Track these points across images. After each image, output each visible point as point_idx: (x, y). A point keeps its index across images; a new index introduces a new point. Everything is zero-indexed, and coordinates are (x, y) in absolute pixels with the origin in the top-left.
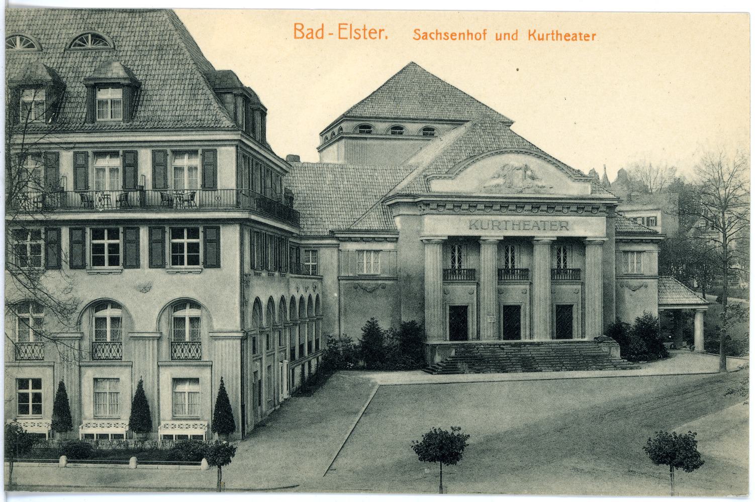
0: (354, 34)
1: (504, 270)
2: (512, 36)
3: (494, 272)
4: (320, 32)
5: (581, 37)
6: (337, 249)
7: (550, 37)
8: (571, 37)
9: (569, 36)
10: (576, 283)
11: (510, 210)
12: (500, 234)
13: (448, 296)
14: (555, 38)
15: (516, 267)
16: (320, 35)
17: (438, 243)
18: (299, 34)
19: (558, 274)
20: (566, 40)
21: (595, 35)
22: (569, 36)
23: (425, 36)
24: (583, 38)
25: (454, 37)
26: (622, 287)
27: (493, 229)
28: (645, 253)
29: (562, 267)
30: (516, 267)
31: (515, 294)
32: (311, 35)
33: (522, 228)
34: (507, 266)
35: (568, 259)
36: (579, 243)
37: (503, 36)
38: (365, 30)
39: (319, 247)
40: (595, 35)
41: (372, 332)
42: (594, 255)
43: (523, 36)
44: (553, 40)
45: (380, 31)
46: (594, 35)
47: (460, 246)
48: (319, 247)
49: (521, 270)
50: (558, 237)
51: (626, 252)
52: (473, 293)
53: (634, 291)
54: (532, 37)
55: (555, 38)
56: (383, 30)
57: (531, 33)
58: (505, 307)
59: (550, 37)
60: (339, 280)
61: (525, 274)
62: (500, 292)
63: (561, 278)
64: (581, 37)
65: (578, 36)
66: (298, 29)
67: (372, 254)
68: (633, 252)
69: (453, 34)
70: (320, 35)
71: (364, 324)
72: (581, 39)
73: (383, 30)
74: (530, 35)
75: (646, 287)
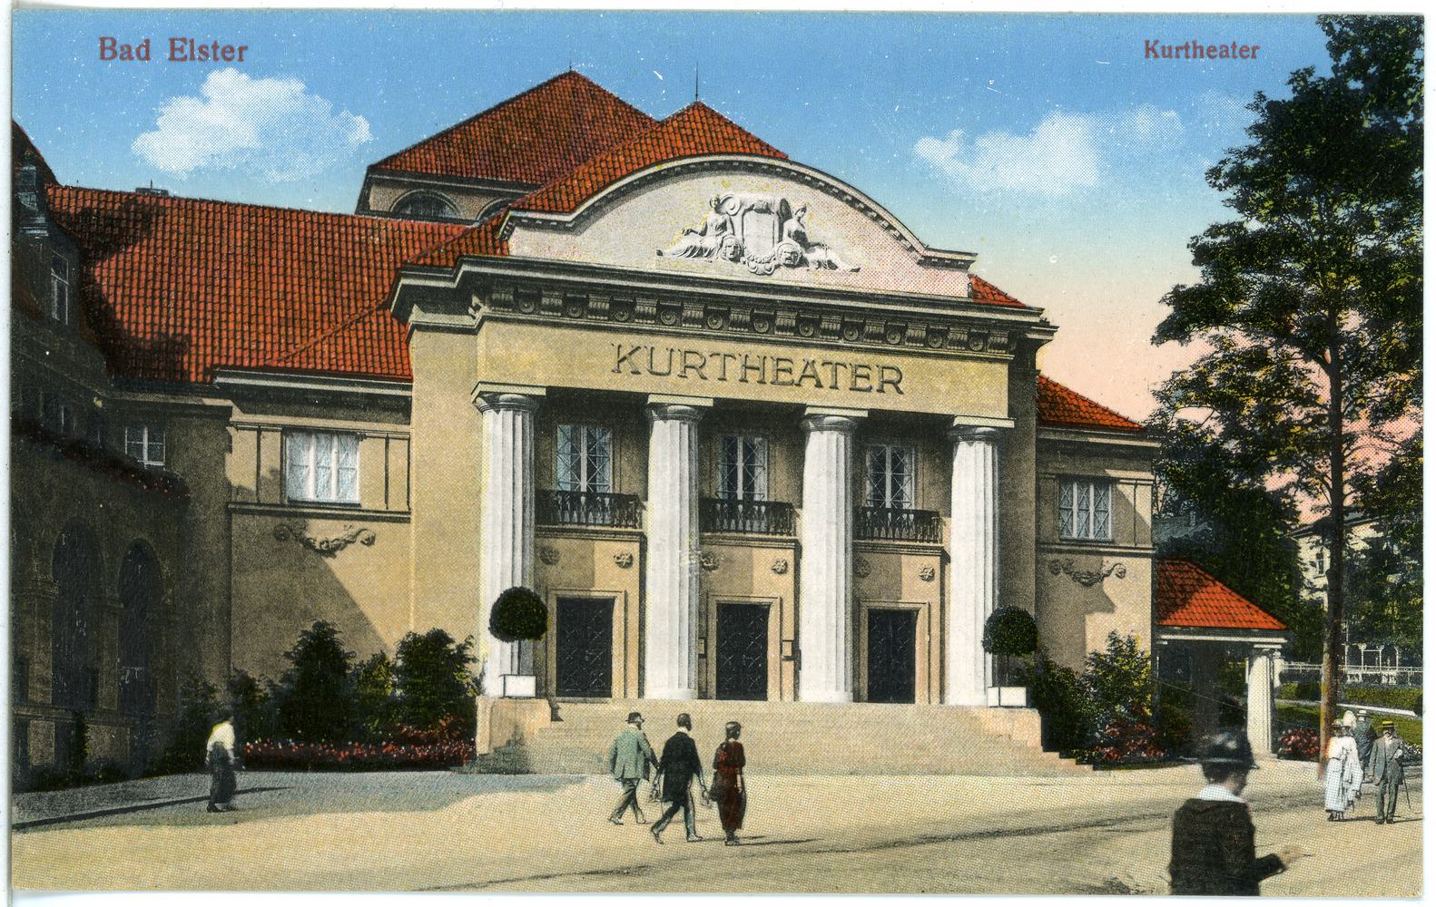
1: (722, 501)
3: (972, 522)
4: (143, 49)
7: (1182, 53)
8: (1219, 51)
9: (1215, 50)
10: (782, 545)
11: (911, 339)
12: (704, 393)
13: (552, 569)
17: (514, 406)
19: (715, 515)
21: (246, 48)
22: (1215, 50)
23: (1168, 53)
25: (229, 55)
27: (881, 391)
30: (906, 506)
32: (127, 54)
33: (769, 377)
36: (935, 437)
40: (246, 48)
42: (972, 469)
43: (161, 52)
44: (1187, 57)
45: (241, 49)
46: (241, 49)
50: (871, 411)
54: (1151, 54)
57: (1151, 45)
59: (1182, 53)
60: (229, 513)
62: (706, 565)
63: (733, 527)
65: (1230, 51)
66: (110, 49)
69: (1212, 49)
70: (143, 54)
71: (292, 642)
74: (1148, 49)
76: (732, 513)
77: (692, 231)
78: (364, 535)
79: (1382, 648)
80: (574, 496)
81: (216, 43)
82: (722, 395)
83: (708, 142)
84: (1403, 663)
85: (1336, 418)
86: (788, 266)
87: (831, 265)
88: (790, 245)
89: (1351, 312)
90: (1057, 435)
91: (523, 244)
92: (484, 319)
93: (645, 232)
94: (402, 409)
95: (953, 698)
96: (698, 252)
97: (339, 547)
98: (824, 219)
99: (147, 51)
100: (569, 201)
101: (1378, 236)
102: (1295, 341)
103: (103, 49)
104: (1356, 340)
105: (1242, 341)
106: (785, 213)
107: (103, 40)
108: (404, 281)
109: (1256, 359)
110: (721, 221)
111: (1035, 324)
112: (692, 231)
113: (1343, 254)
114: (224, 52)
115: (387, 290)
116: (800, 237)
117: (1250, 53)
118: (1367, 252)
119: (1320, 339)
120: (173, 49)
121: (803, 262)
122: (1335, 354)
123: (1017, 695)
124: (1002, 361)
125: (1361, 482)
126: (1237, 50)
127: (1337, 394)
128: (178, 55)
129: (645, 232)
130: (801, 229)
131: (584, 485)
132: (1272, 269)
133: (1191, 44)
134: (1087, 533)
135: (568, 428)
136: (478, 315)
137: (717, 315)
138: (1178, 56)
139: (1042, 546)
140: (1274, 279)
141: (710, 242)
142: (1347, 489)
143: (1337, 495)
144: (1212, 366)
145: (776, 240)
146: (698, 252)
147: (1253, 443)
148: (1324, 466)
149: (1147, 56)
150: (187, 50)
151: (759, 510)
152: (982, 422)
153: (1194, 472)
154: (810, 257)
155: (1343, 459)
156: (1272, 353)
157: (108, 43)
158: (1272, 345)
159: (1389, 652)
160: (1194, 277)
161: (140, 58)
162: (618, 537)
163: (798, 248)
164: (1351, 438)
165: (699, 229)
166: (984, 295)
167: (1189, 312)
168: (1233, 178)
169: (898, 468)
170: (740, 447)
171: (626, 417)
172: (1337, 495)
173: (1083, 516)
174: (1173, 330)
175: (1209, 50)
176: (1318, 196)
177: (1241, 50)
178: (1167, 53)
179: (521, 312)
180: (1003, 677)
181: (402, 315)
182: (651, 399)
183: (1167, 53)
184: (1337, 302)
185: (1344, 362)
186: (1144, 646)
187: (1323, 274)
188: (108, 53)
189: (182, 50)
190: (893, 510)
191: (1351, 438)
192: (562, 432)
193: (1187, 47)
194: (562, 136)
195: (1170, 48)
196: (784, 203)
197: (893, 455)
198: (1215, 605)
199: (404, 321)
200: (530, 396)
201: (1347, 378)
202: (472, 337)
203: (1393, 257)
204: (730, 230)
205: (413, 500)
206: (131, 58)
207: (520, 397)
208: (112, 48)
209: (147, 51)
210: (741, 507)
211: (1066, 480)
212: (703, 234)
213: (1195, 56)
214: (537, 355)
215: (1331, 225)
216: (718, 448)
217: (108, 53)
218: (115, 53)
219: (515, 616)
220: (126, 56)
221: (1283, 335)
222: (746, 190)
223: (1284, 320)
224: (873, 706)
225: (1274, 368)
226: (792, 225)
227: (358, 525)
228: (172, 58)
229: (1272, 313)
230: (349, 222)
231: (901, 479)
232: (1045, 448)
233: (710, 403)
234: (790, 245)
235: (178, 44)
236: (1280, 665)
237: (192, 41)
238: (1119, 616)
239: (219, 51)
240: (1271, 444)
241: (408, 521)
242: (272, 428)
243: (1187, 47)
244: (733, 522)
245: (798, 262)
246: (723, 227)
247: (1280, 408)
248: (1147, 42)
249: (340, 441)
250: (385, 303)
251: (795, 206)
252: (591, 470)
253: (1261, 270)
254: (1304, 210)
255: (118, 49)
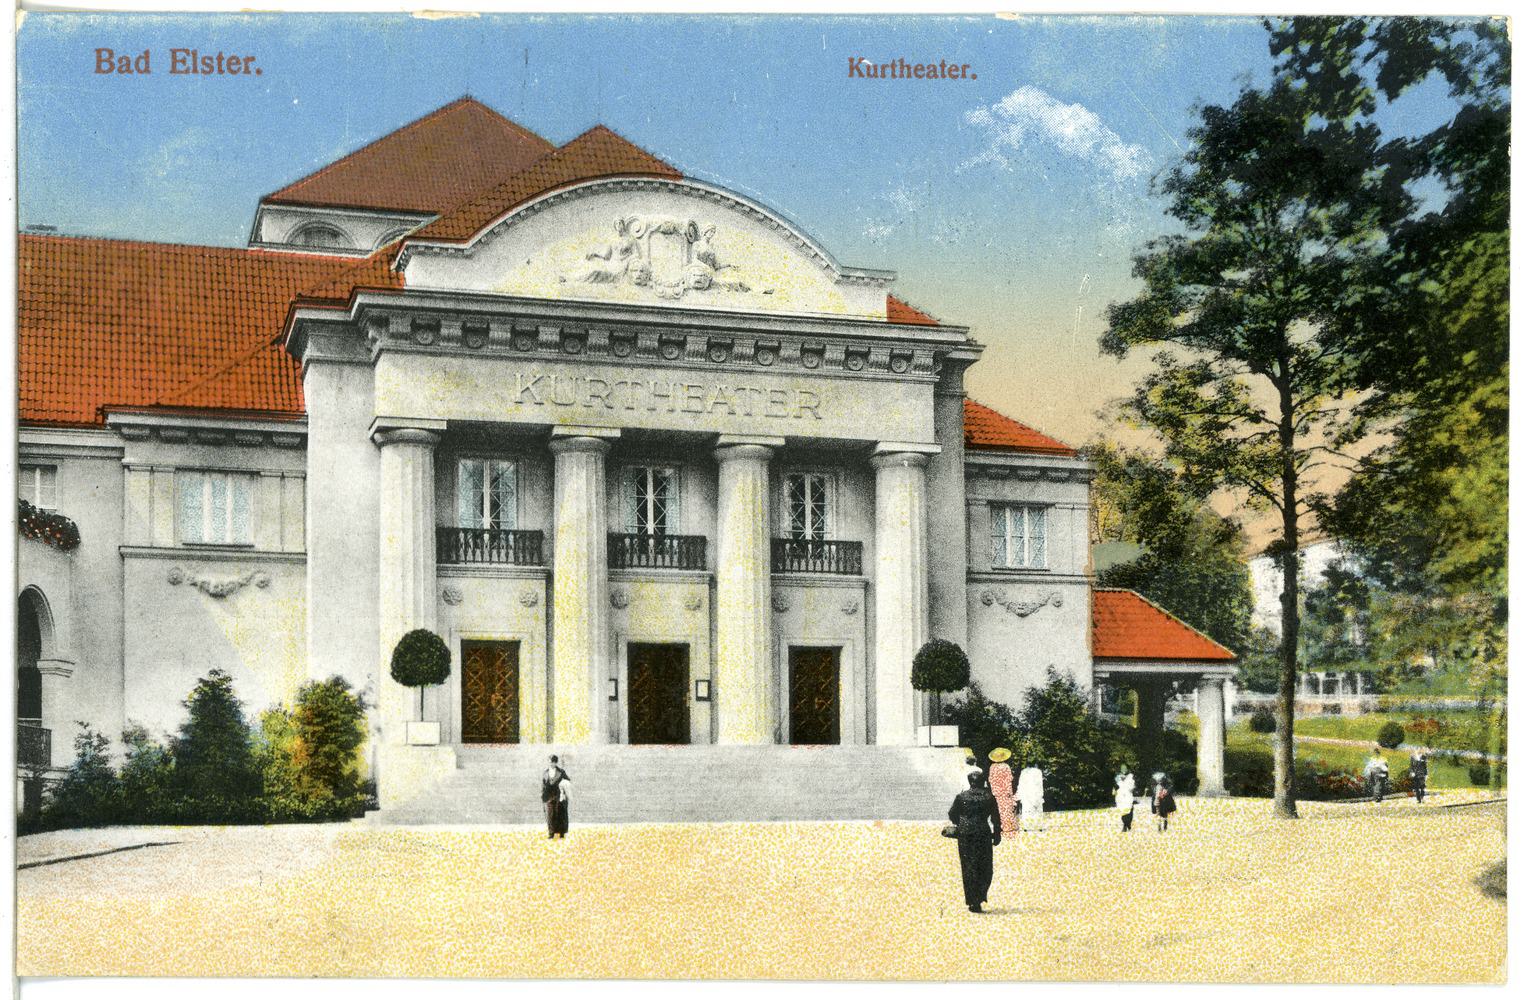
0: (200, 66)
1: (632, 537)
2: (137, 63)
4: (142, 61)
5: (220, 65)
6: (115, 464)
7: (888, 71)
8: (926, 71)
9: (923, 69)
13: (455, 611)
14: (897, 73)
15: (827, 537)
16: (142, 65)
18: (180, 67)
19: (787, 555)
20: (917, 76)
22: (923, 69)
23: (873, 73)
24: (224, 66)
26: (988, 603)
28: (1051, 511)
29: (651, 531)
30: (827, 537)
31: (662, 609)
32: (126, 67)
34: (642, 529)
35: (671, 510)
36: (856, 463)
37: (879, 70)
38: (943, 65)
39: (62, 457)
41: (214, 706)
42: (898, 494)
47: (822, 482)
48: (62, 457)
49: (521, 535)
51: (997, 506)
52: (854, 611)
53: (1022, 616)
54: (855, 72)
55: (897, 73)
56: (253, 59)
58: (792, 649)
59: (888, 71)
61: (694, 553)
64: (220, 65)
66: (106, 61)
67: (1008, 510)
68: (1017, 507)
70: (142, 65)
72: (221, 71)
73: (253, 59)
74: (852, 68)
75: (1058, 605)
76: (644, 549)
77: (596, 256)
78: (260, 577)
79: (1343, 675)
80: (478, 534)
81: (220, 53)
82: (454, 417)
83: (608, 164)
84: (1366, 691)
85: (1286, 432)
86: (697, 289)
87: (743, 288)
88: (698, 268)
89: (1300, 322)
90: (994, 459)
91: (418, 275)
92: (381, 351)
93: (549, 259)
94: (301, 444)
95: (883, 738)
96: (599, 277)
97: (231, 591)
98: (727, 234)
99: (147, 63)
100: (460, 224)
101: (1327, 242)
102: (1241, 356)
103: (99, 61)
104: (1306, 353)
105: (1185, 356)
106: (693, 235)
107: (99, 51)
108: (298, 315)
109: (1203, 376)
110: (625, 245)
111: (961, 343)
112: (596, 256)
113: (1291, 262)
114: (229, 64)
115: (281, 324)
116: (709, 259)
117: (960, 73)
118: (1317, 260)
119: (1266, 351)
120: (175, 61)
121: (711, 285)
122: (1284, 371)
123: (951, 733)
124: (928, 383)
125: (1318, 504)
126: (946, 69)
127: (1287, 408)
128: (180, 67)
129: (549, 259)
130: (711, 251)
131: (487, 522)
132: (1216, 280)
133: (898, 63)
134: (1021, 561)
135: (470, 463)
136: (376, 349)
137: (720, 346)
138: (883, 76)
139: (972, 577)
140: (1217, 290)
141: (614, 266)
142: (1300, 508)
143: (1290, 516)
144: (1152, 383)
145: (685, 261)
146: (599, 277)
147: (1199, 462)
148: (1276, 486)
149: (851, 75)
150: (189, 63)
151: (671, 546)
152: (586, 432)
153: (1151, 501)
154: (719, 278)
155: (1295, 477)
156: (1215, 368)
157: (105, 55)
158: (1217, 359)
159: (1350, 679)
160: (1135, 290)
161: (139, 71)
162: (504, 575)
163: (710, 270)
164: (1303, 456)
165: (603, 253)
166: (898, 314)
167: (1131, 325)
168: (1171, 186)
169: (819, 498)
170: (650, 480)
171: (535, 450)
172: (1290, 516)
173: (1017, 542)
174: (1114, 345)
175: (916, 69)
176: (1264, 204)
177: (950, 70)
178: (872, 72)
179: (518, 350)
180: (938, 716)
181: (296, 350)
182: (557, 431)
183: (872, 72)
184: (1286, 313)
185: (1293, 376)
186: (1084, 678)
187: (1270, 283)
188: (105, 66)
189: (184, 61)
190: (813, 541)
191: (1303, 456)
192: (465, 466)
193: (893, 66)
194: (474, 161)
195: (875, 67)
196: (693, 225)
197: (813, 484)
198: (1159, 634)
199: (297, 358)
200: (602, 438)
201: (1297, 392)
202: (368, 370)
203: (1341, 265)
204: (635, 254)
205: (308, 543)
206: (129, 71)
207: (425, 433)
208: (108, 61)
209: (147, 63)
210: (651, 542)
211: (997, 506)
212: (608, 258)
213: (902, 76)
214: (416, 389)
215: (1278, 232)
216: (787, 488)
217: (105, 66)
218: (112, 64)
219: (418, 660)
220: (124, 68)
221: (1229, 351)
222: (653, 211)
223: (1229, 333)
224: (803, 749)
225: (1218, 384)
226: (701, 246)
227: (252, 567)
228: (174, 70)
229: (1214, 326)
230: (241, 256)
231: (821, 508)
232: (973, 474)
233: (617, 434)
234: (698, 268)
235: (180, 55)
236: (1231, 695)
237: (195, 54)
238: (1038, 649)
239: (224, 64)
240: (1217, 463)
241: (305, 562)
242: (164, 469)
243: (893, 66)
244: (643, 556)
245: (706, 285)
246: (627, 251)
247: (1224, 426)
248: (851, 60)
249: (236, 488)
250: (279, 338)
251: (703, 227)
252: (495, 506)
253: (1201, 281)
254: (1247, 218)
255: (115, 60)
